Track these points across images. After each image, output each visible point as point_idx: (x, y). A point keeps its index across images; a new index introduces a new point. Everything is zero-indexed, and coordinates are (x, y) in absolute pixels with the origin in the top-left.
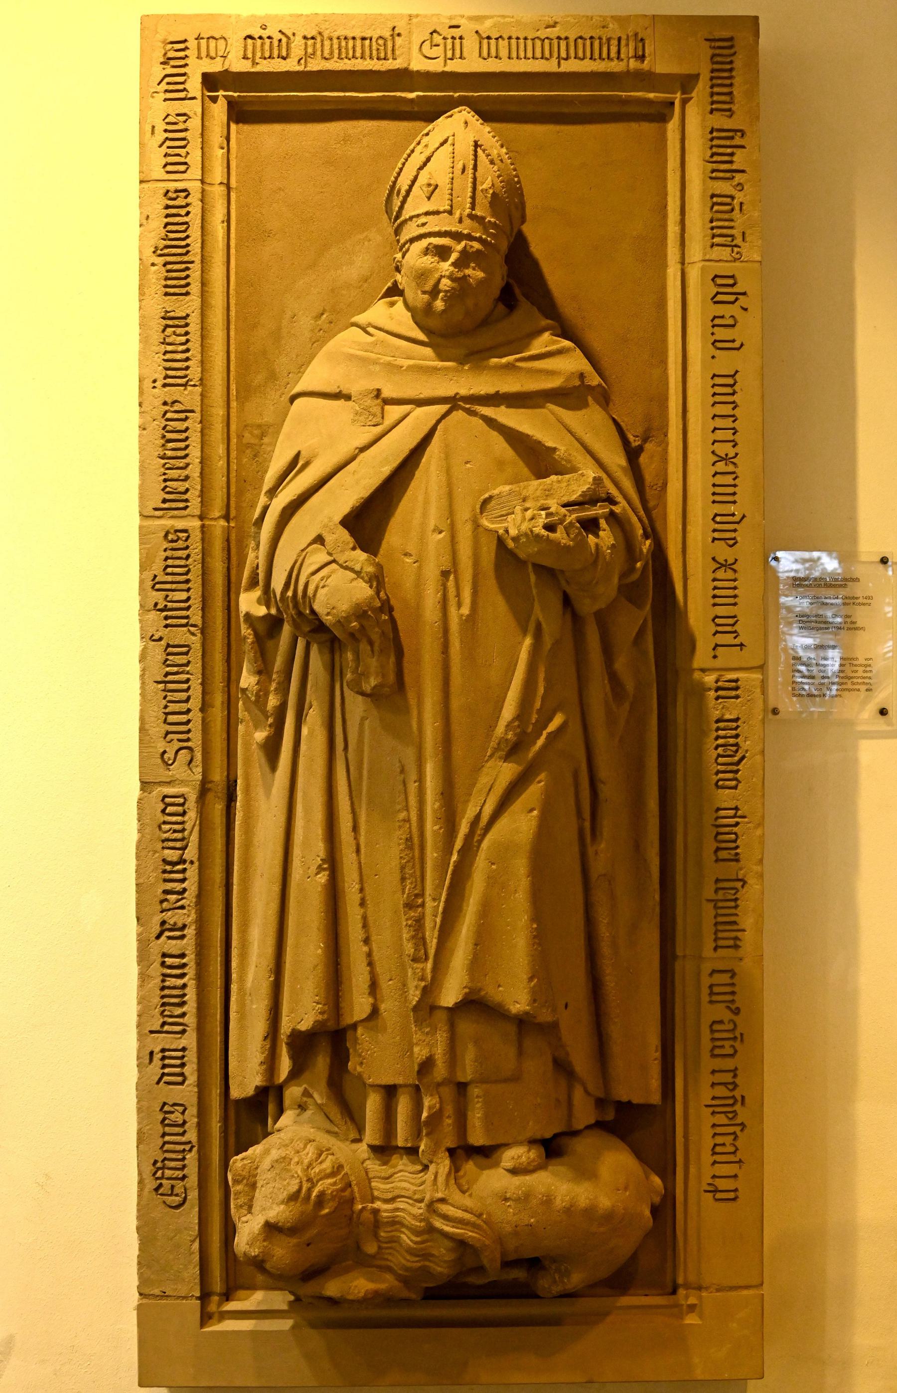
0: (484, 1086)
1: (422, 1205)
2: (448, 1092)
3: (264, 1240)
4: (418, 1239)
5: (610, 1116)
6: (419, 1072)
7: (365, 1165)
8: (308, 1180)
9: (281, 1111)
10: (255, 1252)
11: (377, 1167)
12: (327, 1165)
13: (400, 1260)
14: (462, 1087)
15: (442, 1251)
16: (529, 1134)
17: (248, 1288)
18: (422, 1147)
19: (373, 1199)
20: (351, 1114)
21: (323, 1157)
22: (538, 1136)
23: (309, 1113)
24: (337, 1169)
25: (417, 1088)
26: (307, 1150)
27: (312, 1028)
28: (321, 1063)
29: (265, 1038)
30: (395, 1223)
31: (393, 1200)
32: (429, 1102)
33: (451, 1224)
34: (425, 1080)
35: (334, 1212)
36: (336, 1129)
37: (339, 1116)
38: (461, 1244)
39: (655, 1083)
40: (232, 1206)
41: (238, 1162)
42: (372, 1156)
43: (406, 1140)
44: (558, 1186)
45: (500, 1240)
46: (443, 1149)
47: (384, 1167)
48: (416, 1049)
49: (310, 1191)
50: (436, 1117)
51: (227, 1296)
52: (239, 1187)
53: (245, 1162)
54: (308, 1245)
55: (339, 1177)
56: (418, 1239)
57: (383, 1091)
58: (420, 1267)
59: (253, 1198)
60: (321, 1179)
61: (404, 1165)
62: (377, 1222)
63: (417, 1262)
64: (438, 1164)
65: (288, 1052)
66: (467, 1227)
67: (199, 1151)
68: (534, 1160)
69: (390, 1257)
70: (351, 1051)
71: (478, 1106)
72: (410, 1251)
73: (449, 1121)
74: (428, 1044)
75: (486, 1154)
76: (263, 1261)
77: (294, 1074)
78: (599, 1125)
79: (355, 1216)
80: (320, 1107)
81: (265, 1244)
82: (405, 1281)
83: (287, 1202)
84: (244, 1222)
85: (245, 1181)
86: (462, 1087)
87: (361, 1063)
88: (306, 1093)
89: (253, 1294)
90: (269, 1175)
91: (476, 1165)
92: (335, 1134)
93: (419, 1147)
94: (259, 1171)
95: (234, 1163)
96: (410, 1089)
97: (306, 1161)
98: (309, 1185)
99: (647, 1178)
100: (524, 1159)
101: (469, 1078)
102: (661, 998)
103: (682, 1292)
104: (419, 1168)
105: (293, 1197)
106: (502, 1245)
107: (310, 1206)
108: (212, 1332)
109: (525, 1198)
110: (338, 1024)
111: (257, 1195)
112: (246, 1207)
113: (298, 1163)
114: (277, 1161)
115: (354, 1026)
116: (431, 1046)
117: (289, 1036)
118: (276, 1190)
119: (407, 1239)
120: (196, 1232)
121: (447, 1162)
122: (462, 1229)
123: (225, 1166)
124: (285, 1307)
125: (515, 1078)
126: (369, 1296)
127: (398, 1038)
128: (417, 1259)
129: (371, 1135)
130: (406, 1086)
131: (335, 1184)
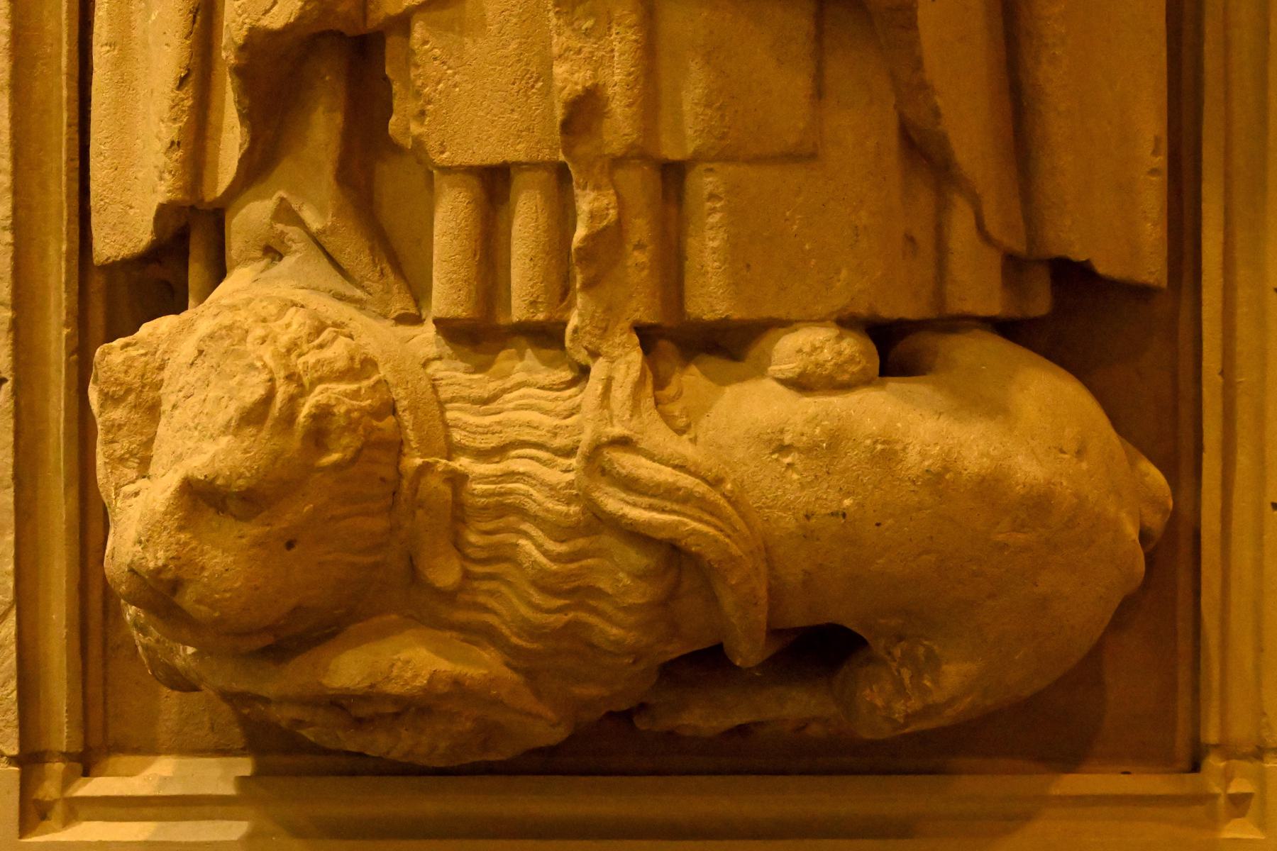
0: (731, 168)
1: (573, 462)
2: (636, 180)
3: (181, 529)
4: (563, 548)
5: (1040, 303)
6: (567, 126)
7: (430, 370)
8: (290, 377)
9: (219, 272)
10: (155, 559)
11: (462, 377)
12: (338, 352)
13: (517, 607)
14: (673, 176)
15: (622, 576)
16: (838, 301)
17: (137, 751)
18: (574, 321)
19: (452, 450)
20: (395, 257)
21: (326, 335)
22: (862, 310)
23: (288, 261)
24: (360, 368)
25: (562, 174)
26: (286, 320)
27: (299, 19)
28: (322, 129)
29: (182, 82)
30: (504, 509)
31: (500, 451)
32: (590, 204)
33: (646, 501)
34: (582, 150)
35: (353, 461)
36: (359, 293)
37: (365, 258)
38: (672, 555)
39: (1152, 230)
40: (100, 460)
41: (114, 356)
42: (448, 350)
43: (533, 303)
44: (913, 423)
45: (767, 551)
46: (626, 325)
47: (476, 376)
48: (560, 70)
49: (293, 401)
50: (608, 240)
51: (86, 761)
52: (118, 414)
53: (132, 352)
54: (290, 545)
55: (365, 383)
56: (563, 548)
57: (474, 182)
58: (567, 625)
59: (151, 441)
60: (321, 380)
61: (529, 371)
62: (459, 512)
63: (559, 610)
64: (612, 361)
65: (239, 102)
66: (688, 509)
67: (16, 392)
68: (851, 360)
69: (492, 603)
70: (396, 87)
71: (715, 219)
72: (544, 583)
73: (641, 257)
74: (588, 60)
75: (728, 345)
76: (176, 585)
77: (256, 168)
78: (1009, 329)
79: (405, 483)
80: (316, 240)
81: (183, 537)
82: (528, 666)
83: (239, 426)
84: (127, 496)
85: (131, 398)
86: (673, 176)
87: (423, 113)
88: (286, 213)
89: (149, 764)
90: (192, 376)
91: (705, 374)
92: (359, 304)
93: (565, 324)
94: (166, 374)
95: (104, 354)
96: (545, 175)
97: (284, 339)
98: (292, 388)
99: (1133, 464)
100: (827, 354)
101: (690, 148)
102: (1169, 49)
103: (1214, 763)
104: (567, 375)
105: (254, 416)
106: (769, 561)
107: (295, 442)
108: (46, 844)
109: (828, 447)
110: (365, 17)
111: (161, 430)
112: (133, 463)
113: (263, 341)
114: (211, 337)
115: (403, 23)
116: (598, 65)
117: (242, 48)
118: (208, 407)
119: (534, 549)
120: (10, 597)
121: (636, 356)
122: (672, 512)
123: (82, 370)
124: (229, 790)
125: (803, 156)
126: (441, 688)
127: (514, 45)
128: (560, 602)
129: (447, 294)
130: (533, 166)
131: (355, 395)
